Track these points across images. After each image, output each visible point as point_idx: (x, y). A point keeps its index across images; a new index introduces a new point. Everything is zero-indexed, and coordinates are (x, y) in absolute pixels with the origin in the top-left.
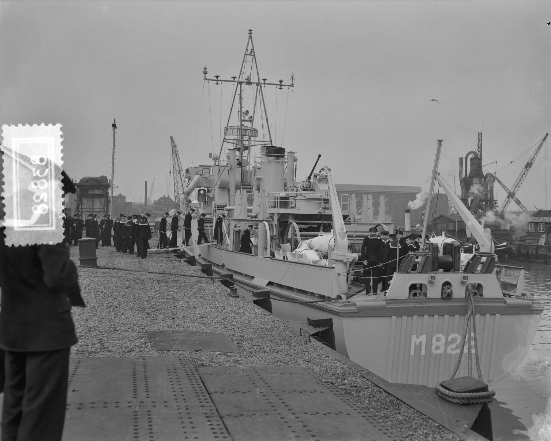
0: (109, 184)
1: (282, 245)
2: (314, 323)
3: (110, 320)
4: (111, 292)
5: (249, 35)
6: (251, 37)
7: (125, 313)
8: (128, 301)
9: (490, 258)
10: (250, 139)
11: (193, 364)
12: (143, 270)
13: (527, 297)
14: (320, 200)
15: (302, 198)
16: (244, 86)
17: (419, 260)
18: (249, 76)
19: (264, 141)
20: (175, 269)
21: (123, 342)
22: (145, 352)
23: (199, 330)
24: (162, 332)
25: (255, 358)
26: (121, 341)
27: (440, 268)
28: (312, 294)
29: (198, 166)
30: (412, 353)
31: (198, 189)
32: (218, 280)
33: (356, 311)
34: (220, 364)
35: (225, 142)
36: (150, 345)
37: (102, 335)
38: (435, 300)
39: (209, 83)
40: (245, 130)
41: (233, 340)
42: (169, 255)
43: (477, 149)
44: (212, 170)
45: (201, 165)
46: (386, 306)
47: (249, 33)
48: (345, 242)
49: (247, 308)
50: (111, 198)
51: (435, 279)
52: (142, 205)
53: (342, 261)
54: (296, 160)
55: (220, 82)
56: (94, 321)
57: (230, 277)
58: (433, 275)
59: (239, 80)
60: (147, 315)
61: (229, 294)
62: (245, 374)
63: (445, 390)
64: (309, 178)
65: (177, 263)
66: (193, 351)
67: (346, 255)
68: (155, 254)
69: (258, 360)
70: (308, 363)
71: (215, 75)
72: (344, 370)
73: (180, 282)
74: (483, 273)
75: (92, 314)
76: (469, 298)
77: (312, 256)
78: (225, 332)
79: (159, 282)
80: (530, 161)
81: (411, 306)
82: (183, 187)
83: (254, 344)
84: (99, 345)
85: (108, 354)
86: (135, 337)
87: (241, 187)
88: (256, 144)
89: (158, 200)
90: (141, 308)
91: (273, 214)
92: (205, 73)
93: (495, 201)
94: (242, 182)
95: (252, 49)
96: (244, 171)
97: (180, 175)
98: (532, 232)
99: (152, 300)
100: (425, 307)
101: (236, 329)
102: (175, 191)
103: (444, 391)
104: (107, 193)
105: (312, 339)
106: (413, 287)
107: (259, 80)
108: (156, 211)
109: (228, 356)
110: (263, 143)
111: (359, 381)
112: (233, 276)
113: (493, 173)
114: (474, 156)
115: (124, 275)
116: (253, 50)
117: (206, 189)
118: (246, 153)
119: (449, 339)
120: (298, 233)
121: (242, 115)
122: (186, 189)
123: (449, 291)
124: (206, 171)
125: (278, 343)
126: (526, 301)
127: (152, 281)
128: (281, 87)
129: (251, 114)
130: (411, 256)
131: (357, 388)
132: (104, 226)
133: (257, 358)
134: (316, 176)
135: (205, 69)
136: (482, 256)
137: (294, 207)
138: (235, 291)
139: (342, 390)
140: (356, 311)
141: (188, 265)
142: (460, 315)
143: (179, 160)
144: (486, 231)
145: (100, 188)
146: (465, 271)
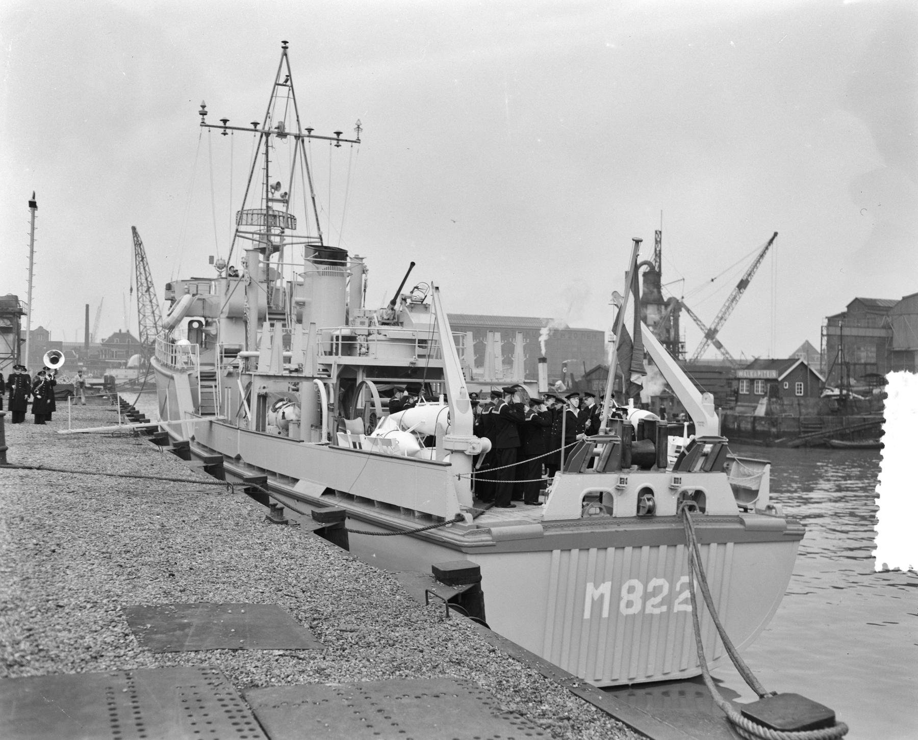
0: (21, 309)
1: (347, 421)
2: (445, 577)
3: (44, 583)
4: (39, 519)
5: (282, 50)
6: (285, 54)
7: (73, 564)
8: (76, 536)
9: (719, 446)
10: (283, 232)
11: (234, 684)
12: (94, 471)
13: (776, 512)
14: (413, 341)
15: (381, 337)
16: (274, 139)
17: (599, 449)
18: (282, 122)
19: (308, 237)
20: (154, 467)
21: (77, 635)
22: (127, 659)
23: (228, 600)
24: (156, 607)
25: (354, 661)
26: (73, 632)
27: (633, 463)
28: (409, 512)
29: (189, 279)
30: (587, 615)
31: (188, 319)
32: (240, 487)
33: (492, 542)
34: (289, 679)
35: (239, 236)
36: (135, 641)
37: (31, 620)
38: (627, 520)
39: (209, 131)
40: (275, 216)
41: (301, 620)
42: (138, 438)
43: (654, 257)
44: (215, 286)
45: (195, 276)
46: (543, 533)
47: (283, 47)
48: (467, 418)
49: (309, 547)
50: (28, 334)
51: (626, 483)
52: (80, 347)
53: (462, 452)
54: (366, 271)
55: (231, 130)
56: (12, 585)
57: (263, 483)
58: (623, 476)
59: (264, 128)
60: (118, 569)
61: (267, 518)
62: (346, 703)
63: (755, 726)
64: (393, 302)
65: (157, 456)
66: (226, 650)
67: (470, 441)
68: (113, 437)
69: (361, 665)
70: (459, 667)
71: (222, 118)
72: (533, 680)
73: (169, 493)
74: (706, 471)
75: (6, 570)
76: (684, 517)
77: (408, 443)
78: (279, 602)
79: (130, 494)
80: (745, 278)
81: (586, 531)
82: (154, 316)
83: (343, 627)
84: (28, 644)
85: (50, 665)
86: (100, 622)
87: (267, 317)
88: (294, 242)
89: (110, 338)
90: (103, 553)
91: (330, 365)
92: (204, 114)
93: (681, 343)
94: (270, 307)
95: (288, 74)
96: (272, 289)
97: (150, 295)
98: (745, 395)
99: (123, 535)
100: (610, 532)
101: (300, 594)
102: (140, 323)
103: (753, 728)
104: (19, 326)
105: (452, 612)
106: (588, 498)
107: (300, 130)
108: (105, 357)
109: (300, 659)
110: (306, 240)
111: (569, 704)
112: (268, 481)
113: (679, 298)
114: (649, 268)
115: (61, 482)
116: (288, 77)
117: (203, 320)
118: (275, 257)
119: (650, 589)
120: (377, 400)
121: (269, 190)
122: (166, 320)
123: (651, 503)
124: (203, 287)
125: (388, 623)
126: (773, 519)
127: (116, 493)
128: (338, 143)
129: (284, 188)
130: (587, 443)
131: (571, 721)
132: (14, 386)
133: (357, 661)
134: (404, 300)
135: (203, 107)
136: (705, 442)
137: (366, 354)
138: (280, 513)
139: (545, 729)
140: (492, 542)
141: (178, 458)
142: (668, 546)
143: (147, 268)
144: (706, 399)
145: (4, 316)
146: (677, 468)
